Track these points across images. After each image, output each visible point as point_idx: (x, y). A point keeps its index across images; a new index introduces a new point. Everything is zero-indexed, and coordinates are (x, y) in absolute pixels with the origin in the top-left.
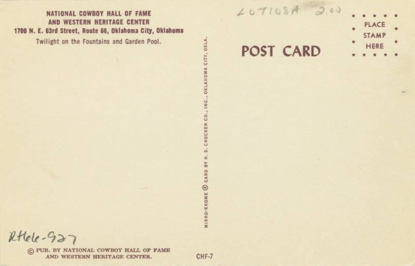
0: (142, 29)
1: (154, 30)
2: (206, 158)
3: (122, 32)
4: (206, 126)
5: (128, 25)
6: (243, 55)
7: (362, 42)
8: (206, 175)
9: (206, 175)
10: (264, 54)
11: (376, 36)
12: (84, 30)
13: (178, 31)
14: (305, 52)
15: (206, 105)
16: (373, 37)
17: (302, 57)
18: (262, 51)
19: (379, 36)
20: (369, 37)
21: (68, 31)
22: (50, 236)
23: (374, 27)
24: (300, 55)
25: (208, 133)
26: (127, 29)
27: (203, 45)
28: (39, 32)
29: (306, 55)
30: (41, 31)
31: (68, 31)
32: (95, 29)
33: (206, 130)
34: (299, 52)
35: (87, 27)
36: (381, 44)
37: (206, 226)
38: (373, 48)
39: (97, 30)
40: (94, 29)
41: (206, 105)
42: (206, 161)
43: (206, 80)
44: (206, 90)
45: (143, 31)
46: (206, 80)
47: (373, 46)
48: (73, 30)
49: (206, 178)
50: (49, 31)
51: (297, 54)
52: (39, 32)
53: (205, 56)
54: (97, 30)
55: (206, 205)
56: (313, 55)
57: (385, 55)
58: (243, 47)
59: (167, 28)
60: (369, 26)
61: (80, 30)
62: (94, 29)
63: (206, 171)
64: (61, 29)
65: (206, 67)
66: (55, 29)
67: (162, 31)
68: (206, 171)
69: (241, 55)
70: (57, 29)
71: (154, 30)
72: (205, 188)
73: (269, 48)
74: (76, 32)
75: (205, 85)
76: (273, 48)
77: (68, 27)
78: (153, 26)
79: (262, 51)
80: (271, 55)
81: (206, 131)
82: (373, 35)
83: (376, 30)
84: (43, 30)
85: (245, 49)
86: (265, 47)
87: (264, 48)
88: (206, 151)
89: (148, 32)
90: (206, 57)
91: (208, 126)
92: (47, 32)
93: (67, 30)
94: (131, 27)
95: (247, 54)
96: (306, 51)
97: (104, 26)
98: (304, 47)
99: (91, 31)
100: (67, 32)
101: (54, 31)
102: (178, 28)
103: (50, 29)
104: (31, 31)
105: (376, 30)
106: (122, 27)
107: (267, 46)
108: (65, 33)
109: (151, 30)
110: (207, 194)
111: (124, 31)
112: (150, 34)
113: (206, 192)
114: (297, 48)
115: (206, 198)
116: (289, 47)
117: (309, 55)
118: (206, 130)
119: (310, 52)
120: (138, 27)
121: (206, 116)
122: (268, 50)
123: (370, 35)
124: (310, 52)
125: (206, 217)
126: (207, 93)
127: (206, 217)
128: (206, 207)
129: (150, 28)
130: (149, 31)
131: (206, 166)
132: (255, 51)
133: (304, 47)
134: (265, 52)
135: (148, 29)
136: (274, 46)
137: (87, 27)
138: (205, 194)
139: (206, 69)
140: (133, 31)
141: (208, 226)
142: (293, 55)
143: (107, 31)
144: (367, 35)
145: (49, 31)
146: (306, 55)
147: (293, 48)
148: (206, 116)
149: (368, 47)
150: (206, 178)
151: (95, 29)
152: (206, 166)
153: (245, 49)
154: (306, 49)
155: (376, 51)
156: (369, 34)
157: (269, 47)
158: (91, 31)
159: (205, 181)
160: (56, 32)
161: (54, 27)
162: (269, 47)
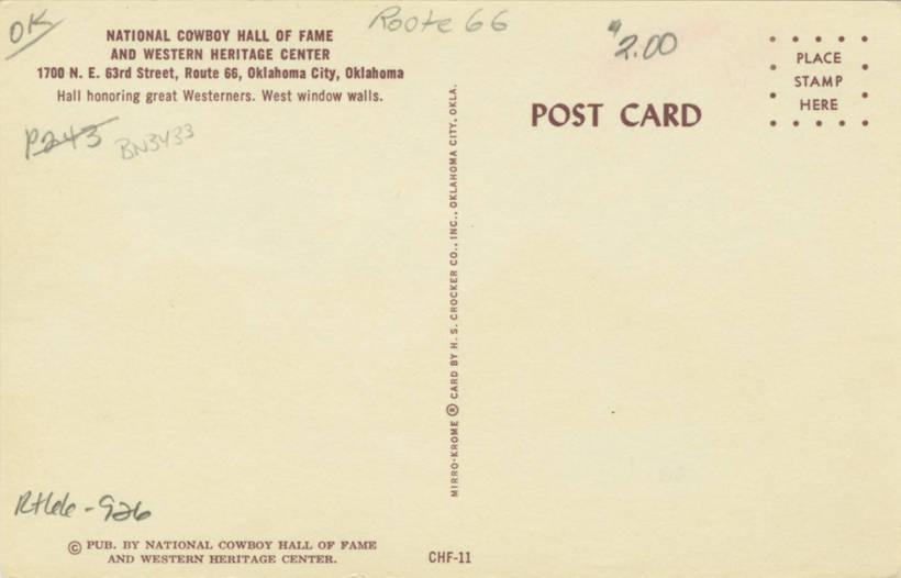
0: (315, 69)
1: (341, 72)
2: (454, 346)
6: (535, 123)
7: (792, 95)
9: (454, 382)
10: (579, 120)
11: (821, 82)
12: (188, 72)
14: (669, 118)
19: (827, 82)
20: (806, 85)
24: (658, 124)
28: (90, 77)
29: (670, 123)
30: (96, 73)
32: (213, 69)
33: (454, 284)
34: (655, 117)
36: (832, 100)
38: (815, 109)
39: (216, 72)
42: (454, 352)
43: (453, 177)
46: (453, 177)
47: (815, 105)
48: (165, 72)
51: (649, 123)
52: (90, 77)
53: (452, 126)
54: (216, 72)
55: (454, 447)
56: (685, 124)
60: (807, 62)
62: (209, 70)
63: (454, 374)
64: (140, 69)
65: (453, 149)
68: (454, 374)
70: (129, 71)
71: (341, 72)
72: (452, 410)
73: (591, 109)
75: (453, 189)
76: (599, 109)
77: (153, 64)
78: (337, 63)
80: (595, 123)
81: (454, 288)
82: (815, 81)
83: (820, 70)
84: (100, 71)
85: (537, 111)
86: (581, 106)
87: (579, 110)
88: (454, 331)
89: (327, 76)
90: (453, 129)
92: (108, 75)
93: (152, 71)
94: (289, 65)
95: (544, 121)
97: (231, 64)
98: (666, 106)
101: (124, 74)
102: (392, 69)
103: (116, 69)
105: (820, 70)
106: (270, 65)
108: (147, 77)
109: (333, 73)
111: (275, 73)
112: (331, 80)
113: (454, 419)
114: (650, 108)
115: (454, 432)
116: (635, 106)
117: (676, 123)
118: (454, 284)
119: (678, 116)
120: (306, 65)
121: (454, 255)
122: (588, 112)
123: (809, 81)
124: (678, 116)
125: (454, 473)
127: (454, 473)
128: (454, 451)
129: (331, 68)
130: (329, 75)
132: (559, 115)
133: (666, 106)
134: (582, 117)
135: (326, 70)
136: (601, 105)
137: (195, 64)
138: (452, 424)
139: (453, 153)
140: (294, 73)
142: (642, 125)
143: (240, 73)
144: (802, 80)
146: (670, 123)
147: (643, 109)
148: (454, 255)
149: (805, 108)
151: (213, 69)
152: (454, 363)
153: (537, 111)
154: (671, 110)
155: (822, 115)
156: (806, 77)
157: (590, 105)
161: (122, 64)
162: (590, 105)
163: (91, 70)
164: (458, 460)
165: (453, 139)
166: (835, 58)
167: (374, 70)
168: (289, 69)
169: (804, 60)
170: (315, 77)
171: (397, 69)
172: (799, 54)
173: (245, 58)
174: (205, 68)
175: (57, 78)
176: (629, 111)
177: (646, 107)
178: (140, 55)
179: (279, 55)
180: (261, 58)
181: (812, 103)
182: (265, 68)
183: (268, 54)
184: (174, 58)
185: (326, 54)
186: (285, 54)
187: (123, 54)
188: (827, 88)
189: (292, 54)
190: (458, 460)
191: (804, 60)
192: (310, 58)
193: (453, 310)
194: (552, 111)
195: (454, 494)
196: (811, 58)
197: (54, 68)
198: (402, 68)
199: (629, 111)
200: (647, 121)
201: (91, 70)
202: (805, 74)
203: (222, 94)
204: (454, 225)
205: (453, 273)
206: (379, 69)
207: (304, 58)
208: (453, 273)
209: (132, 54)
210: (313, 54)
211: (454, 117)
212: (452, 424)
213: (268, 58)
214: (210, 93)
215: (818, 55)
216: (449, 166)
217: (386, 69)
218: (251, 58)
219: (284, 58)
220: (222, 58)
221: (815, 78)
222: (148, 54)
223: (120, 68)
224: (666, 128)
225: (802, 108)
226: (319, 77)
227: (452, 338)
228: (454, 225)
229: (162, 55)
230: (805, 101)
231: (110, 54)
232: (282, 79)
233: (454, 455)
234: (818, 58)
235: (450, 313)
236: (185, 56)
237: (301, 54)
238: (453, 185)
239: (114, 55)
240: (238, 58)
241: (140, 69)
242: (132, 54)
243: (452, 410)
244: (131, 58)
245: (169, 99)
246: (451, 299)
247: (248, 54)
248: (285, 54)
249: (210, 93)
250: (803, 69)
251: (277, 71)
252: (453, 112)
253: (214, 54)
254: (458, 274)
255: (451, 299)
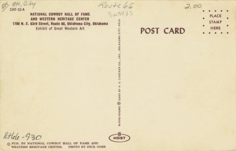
0: (85, 23)
1: (92, 24)
2: (119, 87)
3: (73, 24)
4: (119, 69)
5: (77, 21)
6: (141, 33)
7: (208, 26)
8: (119, 96)
9: (119, 96)
10: (153, 32)
11: (216, 22)
12: (52, 23)
13: (105, 24)
14: (176, 32)
15: (119, 57)
16: (215, 23)
17: (175, 34)
18: (152, 30)
19: (218, 22)
20: (212, 23)
21: (43, 24)
22: (27, 136)
23: (215, 17)
24: (174, 33)
25: (121, 72)
26: (76, 23)
27: (118, 23)
28: (27, 25)
29: (177, 33)
30: (28, 24)
31: (43, 24)
32: (58, 23)
33: (119, 71)
34: (173, 31)
35: (57, 26)
36: (219, 27)
37: (119, 125)
38: (214, 29)
39: (59, 23)
40: (57, 23)
41: (119, 57)
42: (120, 88)
43: (119, 43)
44: (119, 48)
45: (85, 24)
46: (119, 43)
47: (214, 28)
48: (46, 23)
49: (119, 98)
50: (32, 24)
51: (172, 33)
52: (27, 25)
53: (119, 29)
54: (59, 23)
55: (119, 113)
56: (181, 33)
57: (222, 33)
58: (142, 29)
59: (99, 22)
60: (212, 17)
61: (50, 23)
62: (57, 23)
63: (119, 94)
64: (39, 23)
65: (119, 35)
66: (36, 22)
67: (96, 24)
68: (119, 94)
69: (140, 33)
70: (37, 23)
71: (92, 24)
72: (119, 103)
73: (156, 29)
74: (48, 25)
75: (119, 46)
76: (158, 29)
77: (42, 21)
78: (91, 21)
79: (152, 30)
80: (157, 33)
81: (119, 72)
82: (215, 22)
83: (216, 19)
84: (29, 23)
85: (142, 30)
86: (154, 28)
87: (153, 29)
88: (119, 83)
89: (88, 25)
90: (119, 30)
91: (121, 68)
92: (31, 24)
93: (43, 23)
94: (78, 22)
95: (144, 32)
96: (177, 31)
97: (63, 21)
98: (176, 29)
99: (56, 24)
100: (42, 25)
101: (35, 24)
102: (105, 22)
103: (33, 23)
104: (22, 24)
105: (216, 19)
106: (73, 22)
107: (155, 28)
108: (41, 25)
109: (89, 24)
110: (120, 107)
111: (74, 24)
112: (89, 25)
113: (119, 106)
114: (172, 29)
115: (119, 109)
116: (167, 28)
117: (178, 33)
118: (119, 71)
119: (179, 31)
120: (82, 22)
121: (119, 63)
122: (155, 30)
123: (213, 22)
124: (179, 31)
125: (119, 120)
126: (120, 25)
127: (119, 120)
128: (119, 114)
129: (89, 22)
130: (88, 24)
131: (119, 91)
132: (148, 31)
133: (176, 29)
134: (154, 31)
135: (88, 23)
136: (159, 28)
137: (54, 22)
138: (119, 107)
139: (119, 36)
140: (79, 24)
141: (121, 125)
142: (169, 33)
143: (65, 24)
144: (211, 22)
145: (32, 24)
146: (177, 33)
147: (169, 29)
148: (119, 63)
149: (212, 29)
150: (119, 98)
151: (58, 23)
152: (119, 91)
153: (142, 30)
154: (177, 30)
155: (216, 31)
156: (212, 21)
157: (156, 28)
158: (56, 24)
159: (119, 33)
160: (36, 24)
161: (35, 21)
162: (156, 28)
163: (27, 23)
164: (120, 116)
165: (119, 33)
166: (220, 16)
167: (100, 23)
168: (78, 23)
169: (212, 16)
170: (85, 25)
171: (106, 23)
172: (210, 15)
173: (67, 20)
174: (56, 22)
175: (18, 25)
176: (166, 29)
177: (171, 29)
178: (38, 19)
179: (76, 19)
180: (71, 20)
181: (214, 27)
182: (72, 23)
183: (73, 19)
184: (48, 20)
185: (88, 19)
186: (77, 19)
187: (34, 19)
188: (218, 24)
189: (79, 19)
190: (120, 116)
191: (212, 16)
192: (84, 20)
193: (119, 77)
194: (146, 29)
195: (119, 125)
196: (213, 16)
197: (17, 23)
198: (107, 22)
199: (166, 29)
200: (171, 32)
201: (27, 23)
202: (212, 20)
203: (75, 28)
204: (119, 55)
205: (119, 68)
206: (101, 23)
207: (82, 20)
208: (119, 68)
209: (36, 19)
210: (85, 19)
211: (119, 27)
212: (119, 107)
213: (73, 20)
214: (72, 28)
215: (215, 15)
216: (119, 121)
217: (103, 23)
218: (68, 20)
219: (77, 20)
220: (61, 20)
221: (215, 21)
222: (41, 19)
223: (34, 22)
224: (176, 34)
225: (211, 29)
226: (86, 25)
227: (119, 85)
228: (119, 55)
229: (45, 19)
230: (212, 27)
231: (31, 19)
232: (76, 25)
233: (119, 115)
234: (215, 16)
235: (118, 64)
236: (50, 19)
237: (82, 19)
238: (119, 44)
239: (32, 19)
240: (65, 20)
241: (39, 23)
242: (36, 19)
243: (119, 103)
244: (36, 20)
245: (60, 29)
246: (119, 74)
247: (67, 19)
248: (77, 19)
249: (72, 28)
250: (211, 19)
251: (75, 23)
252: (119, 25)
253: (59, 19)
254: (121, 68)
255: (119, 74)
